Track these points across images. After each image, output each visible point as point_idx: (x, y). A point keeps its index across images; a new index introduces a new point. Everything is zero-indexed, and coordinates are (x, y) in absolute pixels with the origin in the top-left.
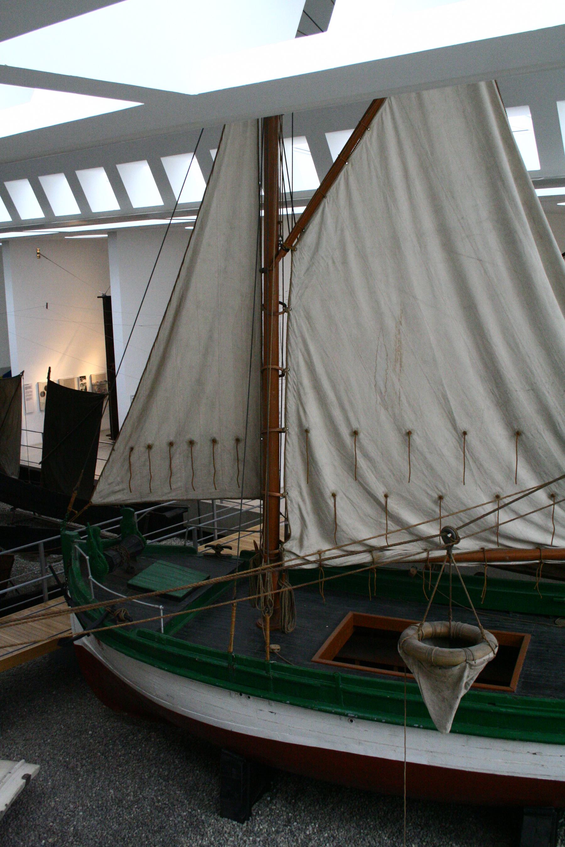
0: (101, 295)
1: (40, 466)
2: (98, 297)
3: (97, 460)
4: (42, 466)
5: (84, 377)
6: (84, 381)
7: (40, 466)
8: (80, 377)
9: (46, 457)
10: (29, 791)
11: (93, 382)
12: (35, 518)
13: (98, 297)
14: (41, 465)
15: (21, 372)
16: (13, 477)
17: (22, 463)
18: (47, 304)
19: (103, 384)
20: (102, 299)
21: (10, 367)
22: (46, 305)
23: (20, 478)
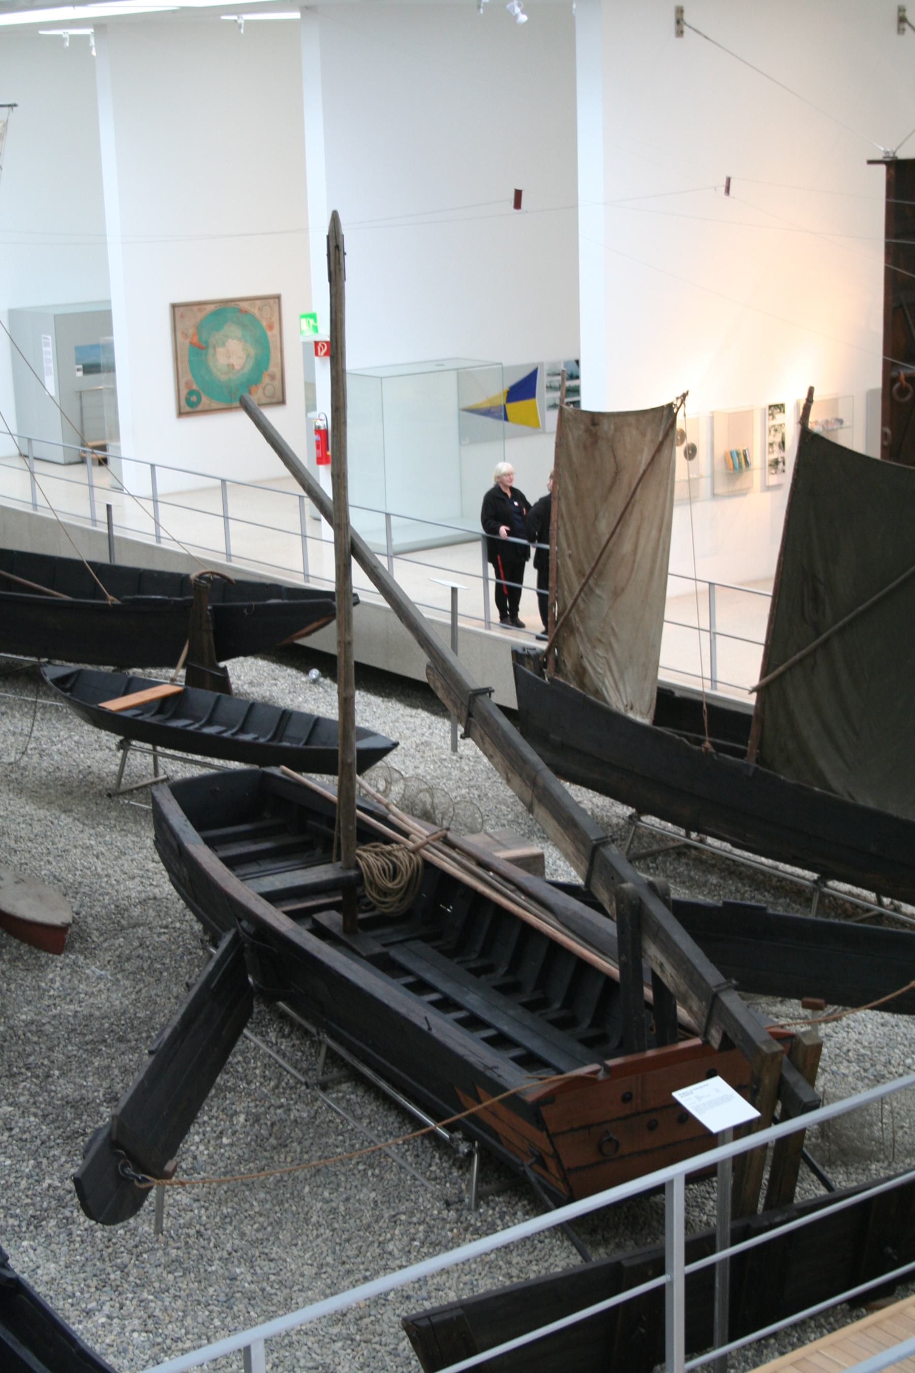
0: (880, 157)
1: (751, 700)
2: (871, 162)
3: (665, 624)
4: (759, 699)
5: (780, 407)
6: (779, 418)
7: (543, 646)
8: (770, 407)
9: (776, 673)
10: (169, 1348)
11: (812, 418)
12: (688, 846)
13: (871, 162)
14: (755, 695)
15: (680, 394)
16: (631, 715)
17: (664, 676)
18: (729, 180)
19: (833, 430)
20: (883, 168)
21: (109, 302)
22: (724, 183)
23: (657, 721)
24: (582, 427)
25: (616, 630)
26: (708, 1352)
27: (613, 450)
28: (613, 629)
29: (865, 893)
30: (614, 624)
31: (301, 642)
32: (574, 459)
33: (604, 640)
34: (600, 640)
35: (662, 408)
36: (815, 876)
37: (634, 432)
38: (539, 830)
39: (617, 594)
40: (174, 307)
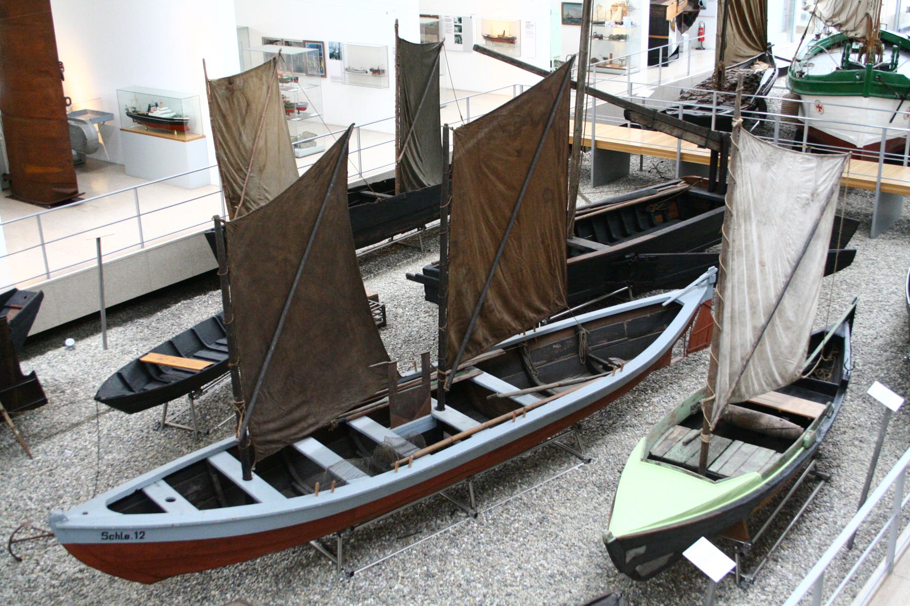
24: (224, 87)
25: (267, 188)
26: (654, 294)
27: (243, 93)
28: (265, 190)
29: (413, 231)
30: (265, 187)
31: (32, 332)
32: (222, 107)
33: (262, 198)
34: (260, 199)
35: (651, 10)
36: (439, 221)
37: (255, 79)
38: (76, 394)
39: (261, 171)
40: (564, 4)
